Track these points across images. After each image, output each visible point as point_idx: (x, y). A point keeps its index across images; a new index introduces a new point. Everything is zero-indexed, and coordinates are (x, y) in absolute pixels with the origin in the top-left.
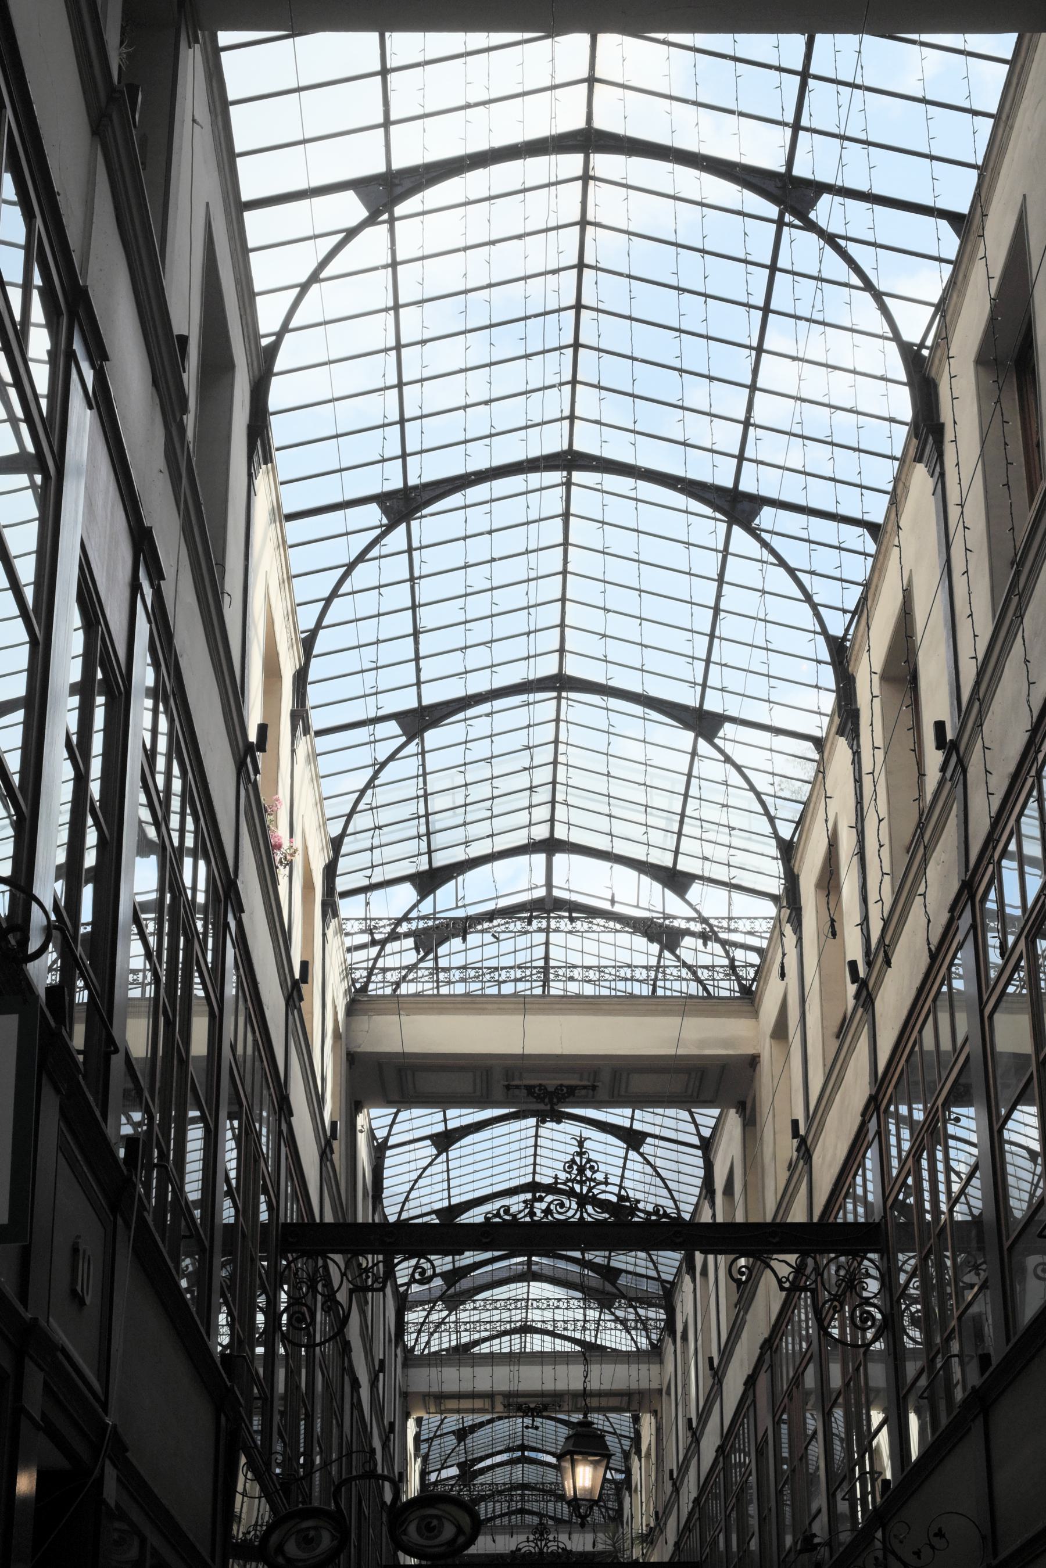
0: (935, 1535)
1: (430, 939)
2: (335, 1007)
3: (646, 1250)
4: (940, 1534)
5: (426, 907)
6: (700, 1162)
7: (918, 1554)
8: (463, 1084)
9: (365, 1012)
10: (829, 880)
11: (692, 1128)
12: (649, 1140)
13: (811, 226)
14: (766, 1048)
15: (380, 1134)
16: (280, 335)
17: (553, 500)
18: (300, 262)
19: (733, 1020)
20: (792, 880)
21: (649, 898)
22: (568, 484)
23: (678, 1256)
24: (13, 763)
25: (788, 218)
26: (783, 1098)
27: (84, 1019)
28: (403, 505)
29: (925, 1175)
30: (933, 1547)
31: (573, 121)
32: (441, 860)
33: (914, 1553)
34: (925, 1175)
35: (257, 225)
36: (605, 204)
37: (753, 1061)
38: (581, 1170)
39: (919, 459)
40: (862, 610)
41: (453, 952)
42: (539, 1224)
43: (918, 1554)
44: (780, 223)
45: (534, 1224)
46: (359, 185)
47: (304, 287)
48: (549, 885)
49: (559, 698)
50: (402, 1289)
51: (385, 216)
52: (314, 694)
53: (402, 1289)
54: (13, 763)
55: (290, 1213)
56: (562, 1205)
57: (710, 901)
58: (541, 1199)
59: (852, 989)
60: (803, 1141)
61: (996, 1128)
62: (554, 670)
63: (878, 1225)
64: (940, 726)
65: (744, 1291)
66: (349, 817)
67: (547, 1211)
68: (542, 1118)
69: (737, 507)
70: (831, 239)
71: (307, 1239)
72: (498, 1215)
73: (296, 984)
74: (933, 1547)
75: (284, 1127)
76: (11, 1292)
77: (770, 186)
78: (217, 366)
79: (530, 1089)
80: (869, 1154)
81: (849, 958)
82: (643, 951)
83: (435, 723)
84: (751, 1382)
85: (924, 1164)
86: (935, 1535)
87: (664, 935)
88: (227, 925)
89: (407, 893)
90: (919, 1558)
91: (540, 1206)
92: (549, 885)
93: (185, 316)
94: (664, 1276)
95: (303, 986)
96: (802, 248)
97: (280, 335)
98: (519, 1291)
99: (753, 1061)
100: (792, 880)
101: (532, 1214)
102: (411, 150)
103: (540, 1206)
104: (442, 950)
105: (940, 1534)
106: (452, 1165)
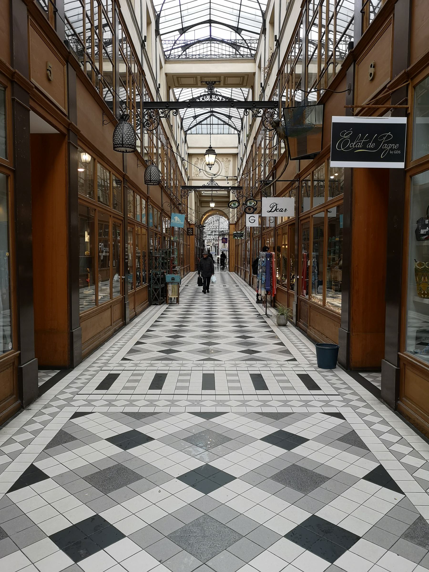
1: (186, 47)
3: (237, 108)
5: (182, 37)
6: (241, 123)
8: (191, 81)
9: (168, 63)
10: (272, 23)
12: (243, 32)
14: (257, 70)
15: (177, 98)
18: (178, 96)
20: (264, 21)
21: (232, 36)
22: (210, 26)
23: (244, 110)
26: (259, 79)
31: (207, 35)
32: (186, 25)
37: (254, 74)
39: (263, 33)
40: (248, 95)
47: (163, 4)
48: (211, 35)
49: (210, 26)
50: (168, 53)
52: (161, 26)
55: (147, 99)
57: (246, 35)
59: (276, 42)
60: (263, 88)
61: (306, 96)
63: (278, 101)
65: (255, 116)
66: (163, 4)
73: (158, 89)
75: (143, 79)
76: (6, 60)
77: (235, 29)
79: (206, 82)
80: (302, 26)
81: (275, 34)
83: (224, 338)
84: (252, 146)
88: (115, 9)
92: (211, 35)
95: (266, 293)
98: (205, 50)
99: (254, 74)
100: (264, 21)
104: (187, 50)
106: (191, 95)
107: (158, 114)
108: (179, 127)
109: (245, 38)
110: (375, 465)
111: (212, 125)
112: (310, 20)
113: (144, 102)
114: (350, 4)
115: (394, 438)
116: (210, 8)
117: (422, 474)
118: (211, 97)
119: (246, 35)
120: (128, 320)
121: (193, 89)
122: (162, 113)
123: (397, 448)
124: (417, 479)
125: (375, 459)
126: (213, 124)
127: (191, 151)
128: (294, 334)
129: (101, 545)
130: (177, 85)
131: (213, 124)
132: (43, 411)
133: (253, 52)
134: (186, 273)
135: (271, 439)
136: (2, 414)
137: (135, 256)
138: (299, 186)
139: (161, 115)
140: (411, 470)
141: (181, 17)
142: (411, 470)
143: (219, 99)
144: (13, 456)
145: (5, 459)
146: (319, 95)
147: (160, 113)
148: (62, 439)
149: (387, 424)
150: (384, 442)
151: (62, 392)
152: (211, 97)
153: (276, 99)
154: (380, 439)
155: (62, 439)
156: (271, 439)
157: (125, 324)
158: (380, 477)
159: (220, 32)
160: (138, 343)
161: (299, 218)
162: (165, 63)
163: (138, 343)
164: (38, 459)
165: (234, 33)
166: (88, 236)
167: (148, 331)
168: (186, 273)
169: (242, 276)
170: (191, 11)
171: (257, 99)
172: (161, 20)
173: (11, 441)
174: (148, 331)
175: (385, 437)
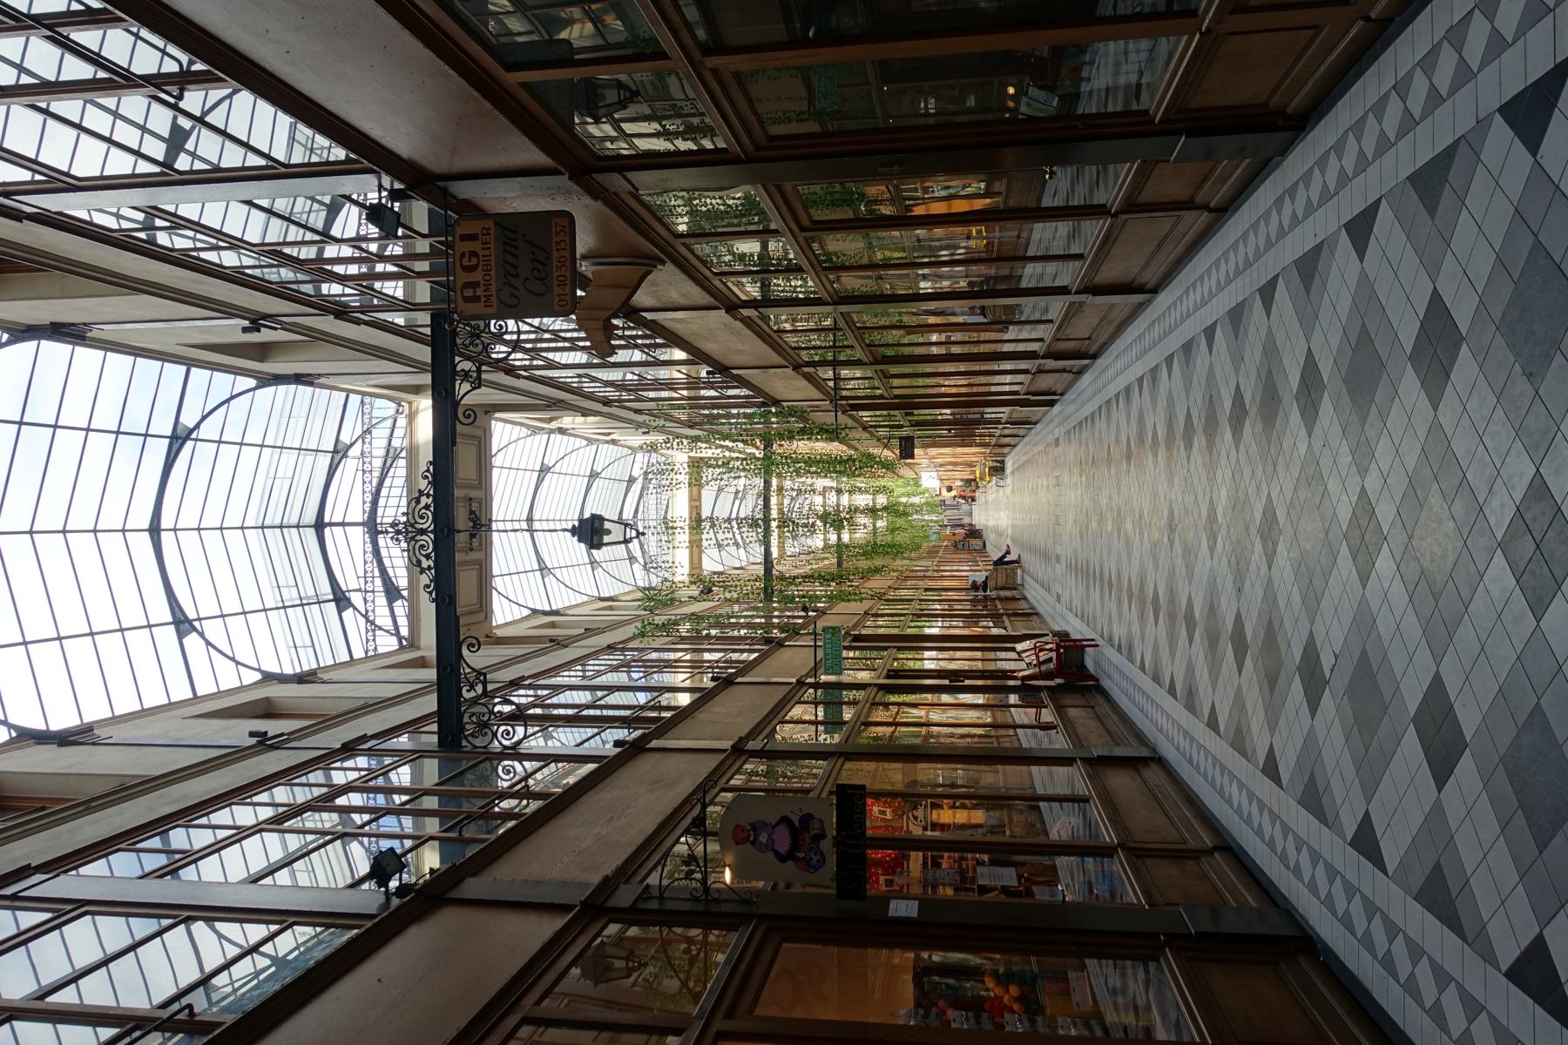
2: (1189, 416)
13: (197, 426)
16: (10, 726)
17: (338, 530)
19: (1245, 206)
22: (331, 524)
24: (107, 1033)
25: (194, 436)
28: (183, 624)
32: (325, 589)
35: (205, 687)
36: (189, 519)
38: (398, 532)
41: (402, 582)
44: (196, 440)
45: (436, 567)
46: (340, 611)
49: (331, 524)
51: (196, 624)
54: (107, 1033)
56: (422, 547)
58: (419, 562)
62: (312, 530)
64: (245, 330)
67: (428, 557)
68: (490, 529)
69: (544, 470)
70: (204, 418)
71: (768, 593)
78: (267, 710)
82: (350, 466)
88: (370, 749)
89: (636, 566)
91: (425, 563)
93: (239, 732)
96: (209, 430)
97: (10, 726)
100: (278, 379)
101: (429, 568)
102: (162, 613)
103: (425, 563)
107: (474, 701)
109: (358, 432)
110: (1498, 120)
111: (537, 525)
115: (1394, 108)
116: (263, 527)
117: (1509, 15)
118: (423, 532)
119: (636, 473)
120: (1144, 752)
121: (496, 571)
122: (472, 687)
123: (1416, 103)
124: (1521, 31)
125: (1483, 124)
126: (530, 519)
128: (1175, 303)
129: (1546, 728)
131: (530, 519)
132: (1279, 850)
134: (1023, 605)
135: (1310, 413)
136: (1362, 1039)
137: (988, 194)
139: (479, 689)
140: (1497, 45)
141: (284, 607)
142: (1497, 45)
143: (427, 507)
144: (1473, 1008)
145: (1481, 1029)
147: (473, 694)
148: (1440, 895)
149: (1434, 51)
150: (1456, 87)
151: (1313, 887)
152: (423, 532)
153: (424, 318)
154: (1422, 120)
155: (1440, 895)
156: (1310, 413)
157: (1160, 761)
158: (1360, 229)
159: (348, 501)
160: (1212, 724)
162: (418, 648)
163: (1172, 691)
164: (1489, 957)
167: (1142, 668)
168: (1023, 605)
169: (1021, 432)
170: (285, 577)
171: (427, 379)
172: (539, 607)
173: (1437, 1014)
174: (1142, 668)
175: (1391, 130)
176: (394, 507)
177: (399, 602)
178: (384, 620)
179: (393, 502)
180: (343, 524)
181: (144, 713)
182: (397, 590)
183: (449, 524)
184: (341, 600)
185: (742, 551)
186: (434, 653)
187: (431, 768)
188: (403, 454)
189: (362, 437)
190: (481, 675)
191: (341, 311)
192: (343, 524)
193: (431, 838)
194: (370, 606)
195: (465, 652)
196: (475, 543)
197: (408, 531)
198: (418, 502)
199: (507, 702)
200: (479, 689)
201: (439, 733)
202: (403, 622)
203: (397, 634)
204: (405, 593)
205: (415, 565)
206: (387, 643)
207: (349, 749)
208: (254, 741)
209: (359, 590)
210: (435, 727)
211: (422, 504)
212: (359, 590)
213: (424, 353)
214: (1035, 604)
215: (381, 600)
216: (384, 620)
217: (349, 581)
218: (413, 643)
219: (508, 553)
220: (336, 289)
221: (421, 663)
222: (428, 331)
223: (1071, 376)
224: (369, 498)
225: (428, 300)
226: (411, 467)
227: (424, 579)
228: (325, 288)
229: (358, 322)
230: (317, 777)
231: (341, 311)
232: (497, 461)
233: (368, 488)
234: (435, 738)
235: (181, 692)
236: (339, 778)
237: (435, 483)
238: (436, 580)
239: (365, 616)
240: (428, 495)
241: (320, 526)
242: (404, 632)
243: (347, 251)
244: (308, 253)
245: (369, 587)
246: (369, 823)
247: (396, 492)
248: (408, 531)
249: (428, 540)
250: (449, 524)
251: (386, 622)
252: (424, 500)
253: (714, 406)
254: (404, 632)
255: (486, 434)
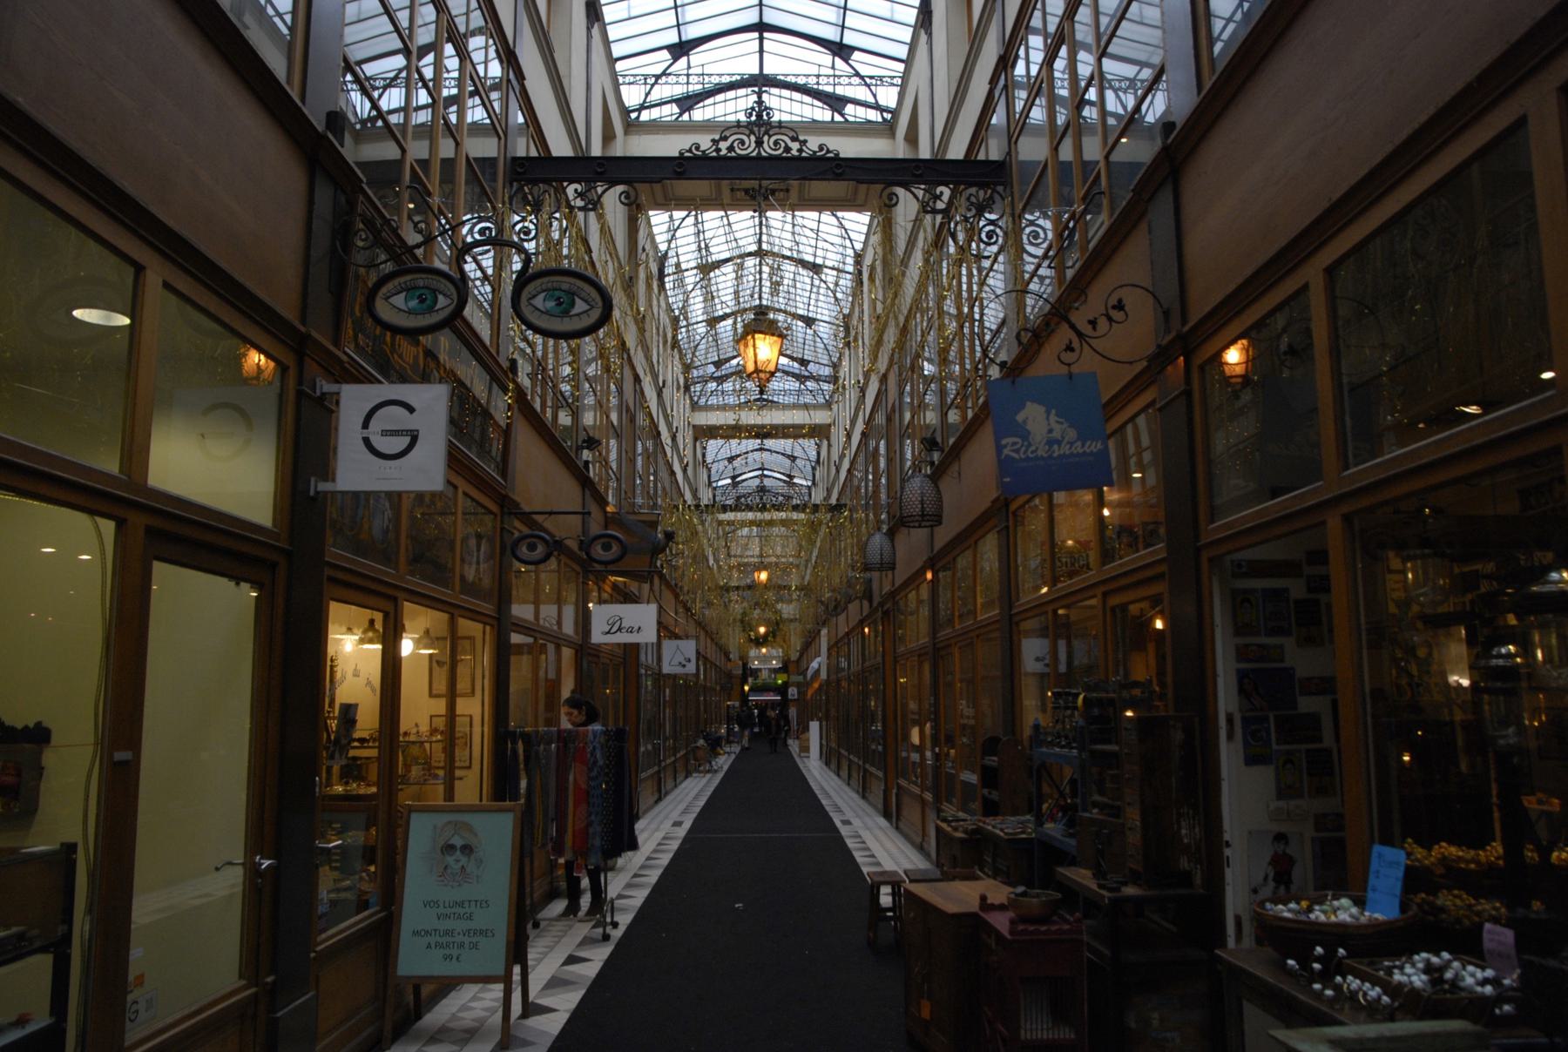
0: (1114, 307)
4: (1120, 306)
7: (1093, 323)
9: (638, 133)
11: (847, 224)
22: (761, 39)
26: (838, 436)
27: (135, 937)
29: (964, 279)
30: (1110, 319)
31: (755, 19)
32: (691, 33)
33: (1090, 322)
34: (964, 279)
41: (699, 114)
42: (725, 158)
43: (1093, 323)
45: (720, 158)
46: (669, 48)
49: (761, 39)
50: (633, 115)
53: (633, 115)
56: (743, 143)
58: (725, 139)
67: (731, 148)
72: (690, 151)
74: (1110, 319)
85: (964, 272)
86: (1114, 307)
87: (800, 378)
89: (711, 369)
90: (1094, 329)
91: (723, 145)
94: (882, 102)
101: (718, 150)
103: (723, 145)
105: (1120, 306)
108: (665, 342)
109: (864, 70)
112: (1018, 109)
113: (515, 159)
114: (1148, 31)
118: (759, 143)
119: (811, 367)
122: (580, 195)
127: (704, 419)
130: (660, 198)
133: (888, 116)
134: (670, 783)
138: (1188, 394)
143: (787, 149)
146: (964, 416)
152: (759, 143)
153: (993, 150)
157: (660, 799)
159: (786, 58)
161: (1011, 616)
162: (626, 133)
165: (826, 58)
166: (1264, 776)
171: (925, 153)
176: (786, 107)
177: (676, 109)
178: (661, 92)
179: (786, 105)
180: (761, 51)
181: (650, 226)
182: (690, 109)
183: (762, 171)
184: (681, 49)
185: (729, 481)
186: (619, 153)
187: (485, 148)
188: (838, 118)
189: (857, 74)
190: (594, 205)
191: (1005, 62)
192: (761, 51)
193: (404, 151)
194: (672, 79)
195: (620, 188)
196: (740, 194)
197: (760, 123)
198: (794, 139)
199: (563, 232)
200: (579, 203)
201: (528, 159)
202: (654, 114)
203: (642, 107)
204: (686, 117)
205: (725, 130)
206: (632, 96)
207: (509, 57)
208: (505, 365)
209: (689, 67)
210: (534, 153)
211: (791, 144)
212: (689, 67)
213: (957, 151)
214: (670, 798)
215: (679, 91)
216: (659, 93)
217: (697, 57)
218: (632, 126)
219: (732, 229)
220: (1037, 57)
221: (608, 136)
222: (981, 157)
223: (919, 840)
224: (802, 81)
225: (1022, 157)
226: (815, 126)
227: (705, 142)
228: (1036, 41)
229: (993, 81)
230: (477, 20)
231: (1005, 62)
232: (826, 217)
233: (812, 80)
234: (521, 153)
235: (617, 50)
236: (476, 42)
237: (814, 158)
238: (705, 158)
239: (664, 73)
240: (800, 151)
241: (761, 27)
242: (645, 116)
243: (1084, 70)
244: (1083, 32)
245: (693, 79)
246: (422, 78)
247: (797, 108)
248: (760, 123)
249: (750, 148)
250: (762, 171)
251: (656, 94)
252: (795, 146)
253: (889, 461)
254: (645, 116)
255: (858, 207)
